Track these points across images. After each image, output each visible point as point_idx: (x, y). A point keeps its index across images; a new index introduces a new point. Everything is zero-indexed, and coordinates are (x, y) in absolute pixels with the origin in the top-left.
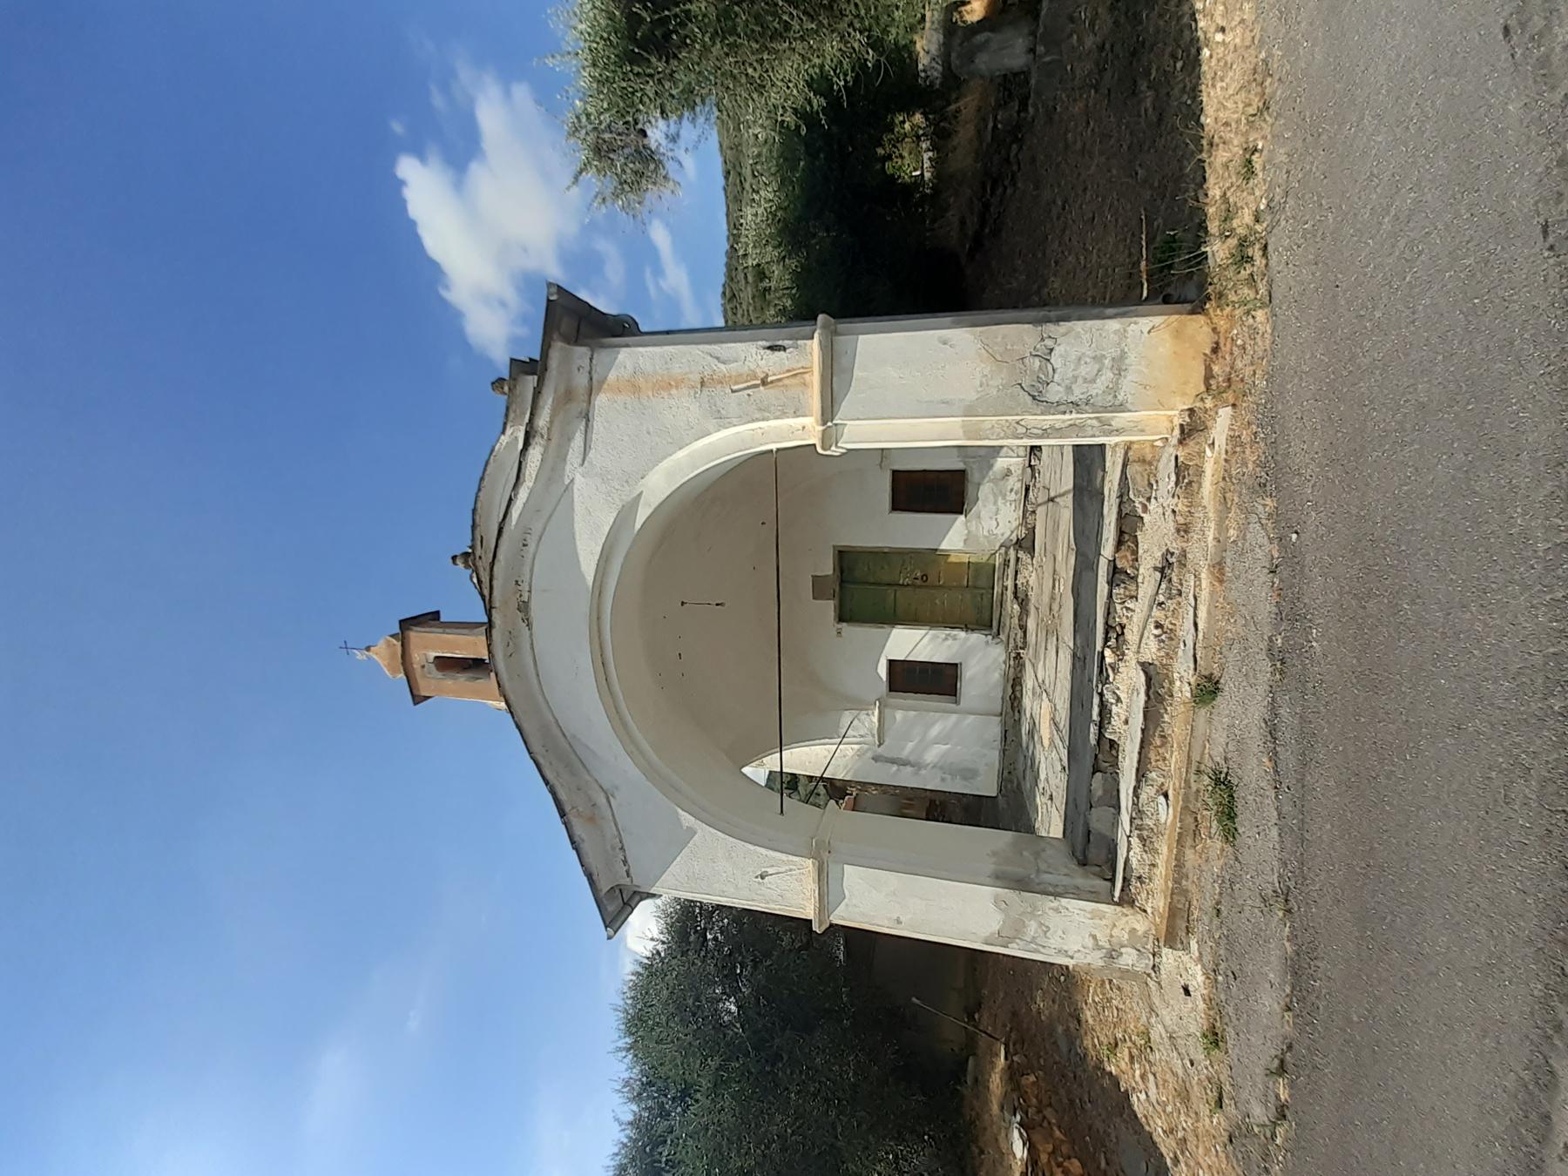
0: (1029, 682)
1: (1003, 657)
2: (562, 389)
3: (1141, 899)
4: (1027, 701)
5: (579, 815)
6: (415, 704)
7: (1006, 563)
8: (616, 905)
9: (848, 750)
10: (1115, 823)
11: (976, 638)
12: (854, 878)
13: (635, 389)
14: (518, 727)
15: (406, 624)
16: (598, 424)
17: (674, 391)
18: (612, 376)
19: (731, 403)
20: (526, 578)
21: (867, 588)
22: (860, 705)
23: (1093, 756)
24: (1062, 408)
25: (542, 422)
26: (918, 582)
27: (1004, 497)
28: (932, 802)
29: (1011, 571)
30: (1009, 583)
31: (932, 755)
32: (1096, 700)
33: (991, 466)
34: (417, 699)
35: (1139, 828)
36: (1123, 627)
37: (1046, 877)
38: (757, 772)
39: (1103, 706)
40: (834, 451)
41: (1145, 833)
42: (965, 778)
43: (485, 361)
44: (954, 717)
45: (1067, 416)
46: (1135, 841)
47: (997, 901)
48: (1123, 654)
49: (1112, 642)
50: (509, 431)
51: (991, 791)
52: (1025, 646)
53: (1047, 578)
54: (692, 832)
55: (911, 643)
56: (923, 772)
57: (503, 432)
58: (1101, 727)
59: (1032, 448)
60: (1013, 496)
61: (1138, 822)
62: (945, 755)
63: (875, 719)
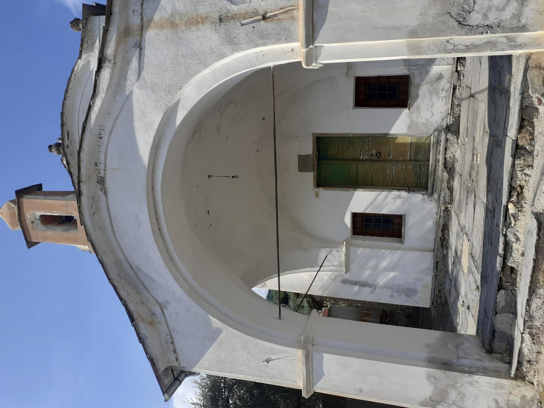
0: (454, 228)
1: (435, 211)
2: (122, 28)
3: (530, 376)
4: (453, 240)
5: (143, 320)
6: (29, 247)
7: (438, 142)
8: (170, 378)
9: (325, 276)
10: (513, 324)
11: (418, 197)
12: (330, 362)
13: (172, 24)
14: (101, 262)
15: (21, 193)
16: (148, 51)
17: (200, 26)
18: (157, 17)
19: (241, 32)
20: (102, 160)
21: (336, 163)
22: (332, 244)
23: (498, 279)
24: (481, 30)
25: (110, 51)
26: (374, 158)
27: (437, 94)
28: (384, 312)
29: (442, 148)
30: (441, 157)
31: (382, 281)
32: (502, 239)
33: (427, 72)
34: (30, 244)
35: (530, 327)
36: (522, 187)
37: (464, 362)
38: (261, 290)
39: (507, 245)
40: (315, 66)
41: (534, 331)
42: (407, 295)
43: (66, 9)
44: (398, 253)
45: (484, 36)
46: (527, 336)
47: (429, 377)
48: (522, 207)
49: (514, 199)
50: (84, 56)
51: (428, 306)
52: (451, 201)
53: (469, 152)
54: (219, 332)
55: (364, 201)
56: (377, 291)
57: (80, 57)
58: (505, 258)
59: (459, 59)
60: (444, 94)
61: (529, 323)
62: (394, 278)
63: (343, 257)
